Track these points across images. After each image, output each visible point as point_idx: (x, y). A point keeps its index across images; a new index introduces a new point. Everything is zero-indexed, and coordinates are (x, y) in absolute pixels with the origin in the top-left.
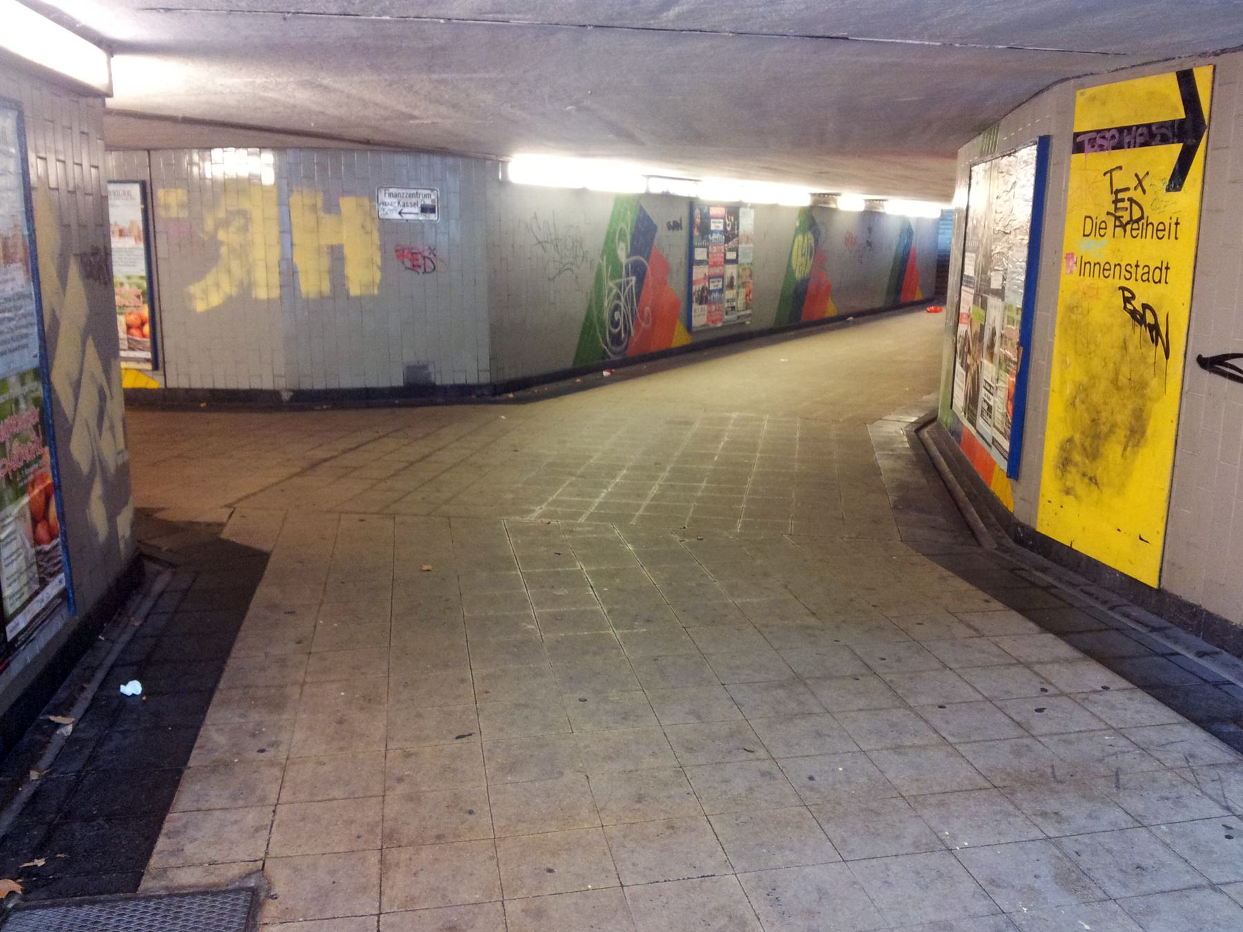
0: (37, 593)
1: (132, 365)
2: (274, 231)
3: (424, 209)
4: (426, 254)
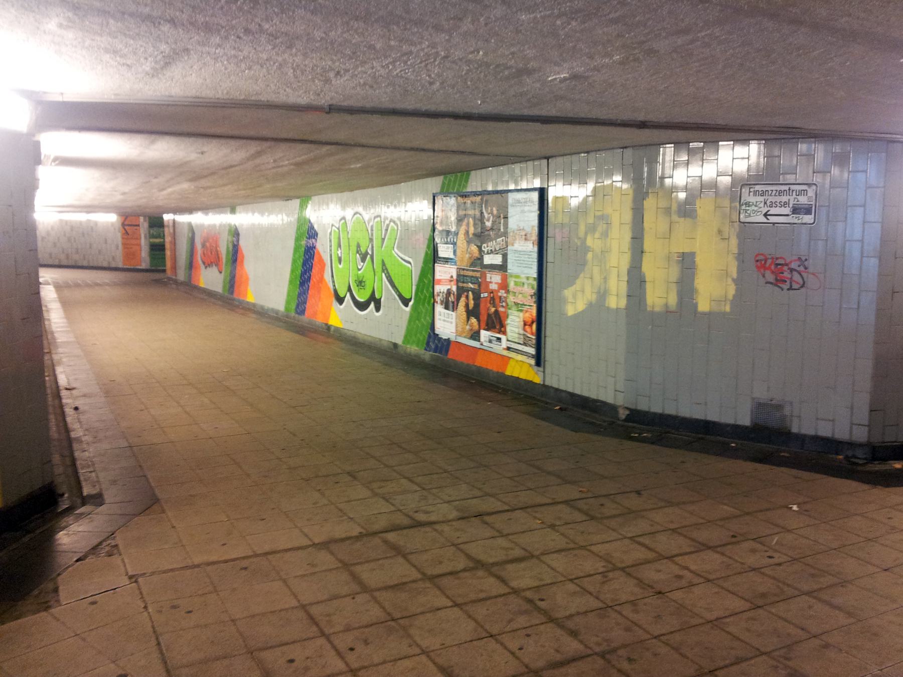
1: (520, 357)
2: (627, 236)
3: (796, 210)
4: (794, 265)
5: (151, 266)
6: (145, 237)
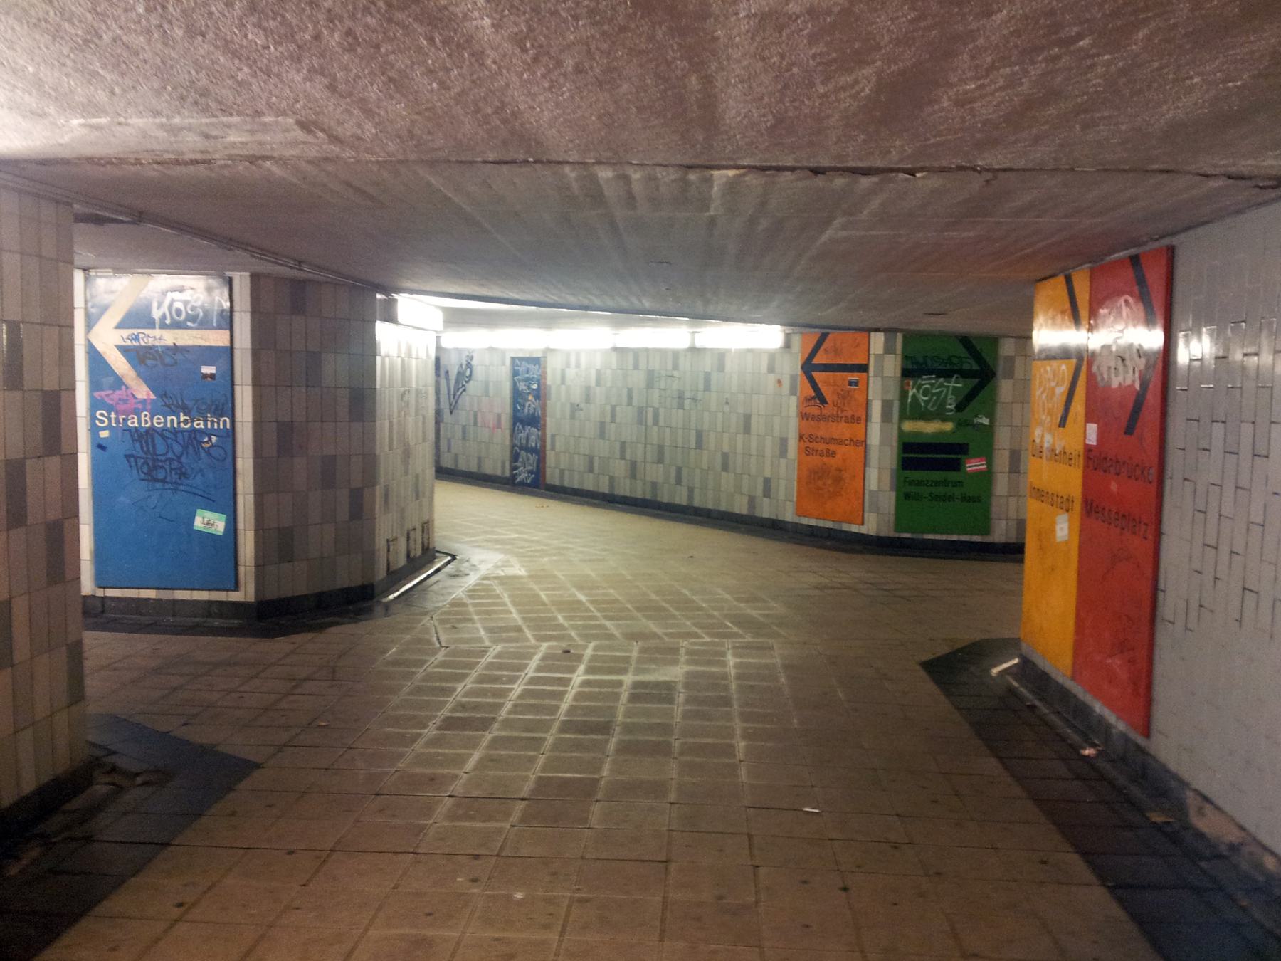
5: (898, 526)
6: (886, 417)
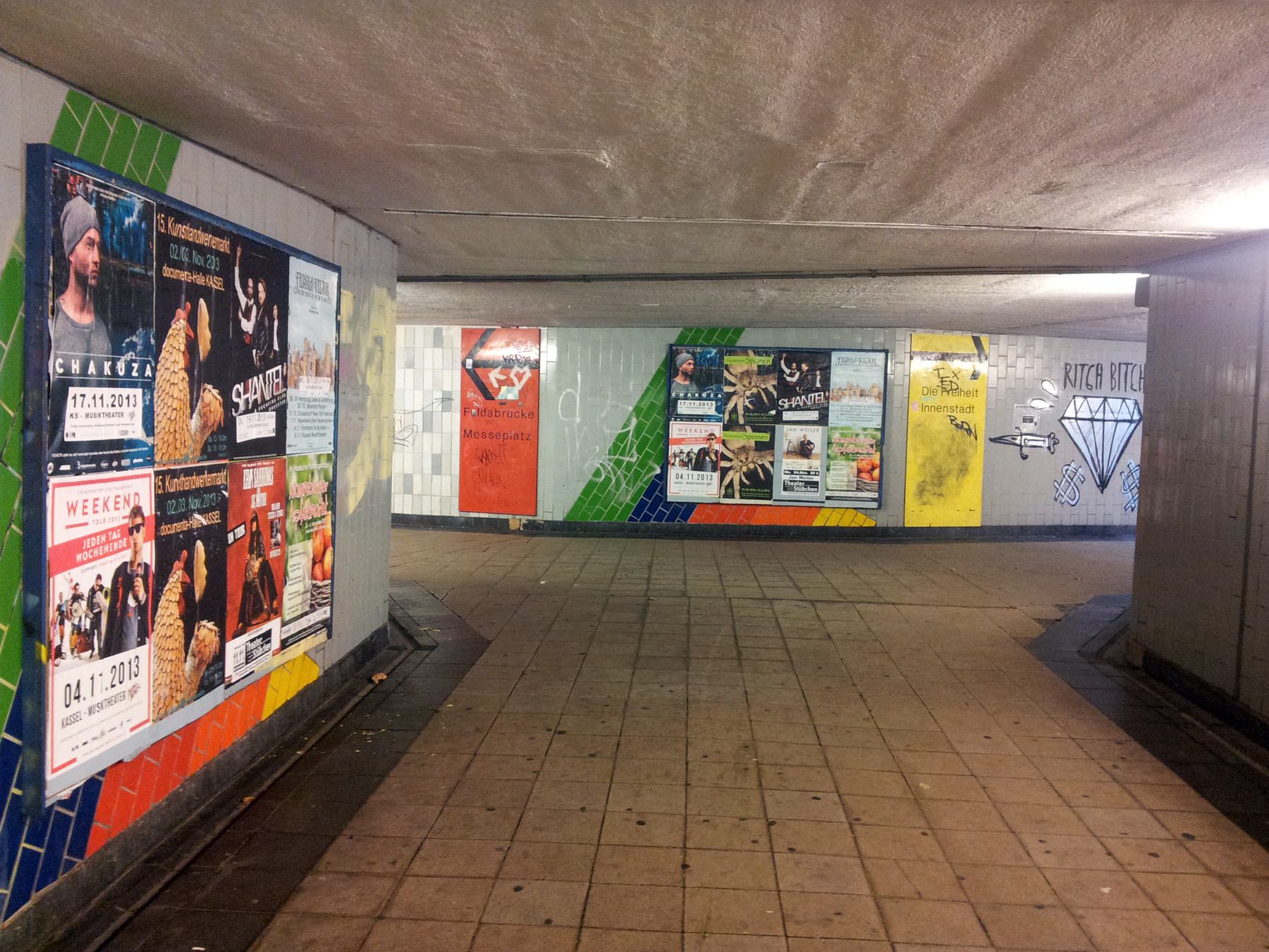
0: (306, 614)
